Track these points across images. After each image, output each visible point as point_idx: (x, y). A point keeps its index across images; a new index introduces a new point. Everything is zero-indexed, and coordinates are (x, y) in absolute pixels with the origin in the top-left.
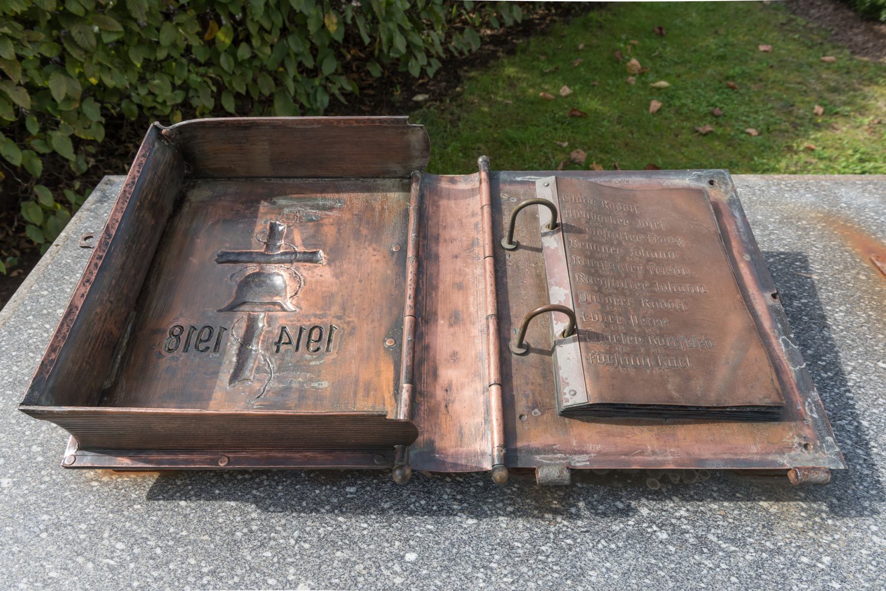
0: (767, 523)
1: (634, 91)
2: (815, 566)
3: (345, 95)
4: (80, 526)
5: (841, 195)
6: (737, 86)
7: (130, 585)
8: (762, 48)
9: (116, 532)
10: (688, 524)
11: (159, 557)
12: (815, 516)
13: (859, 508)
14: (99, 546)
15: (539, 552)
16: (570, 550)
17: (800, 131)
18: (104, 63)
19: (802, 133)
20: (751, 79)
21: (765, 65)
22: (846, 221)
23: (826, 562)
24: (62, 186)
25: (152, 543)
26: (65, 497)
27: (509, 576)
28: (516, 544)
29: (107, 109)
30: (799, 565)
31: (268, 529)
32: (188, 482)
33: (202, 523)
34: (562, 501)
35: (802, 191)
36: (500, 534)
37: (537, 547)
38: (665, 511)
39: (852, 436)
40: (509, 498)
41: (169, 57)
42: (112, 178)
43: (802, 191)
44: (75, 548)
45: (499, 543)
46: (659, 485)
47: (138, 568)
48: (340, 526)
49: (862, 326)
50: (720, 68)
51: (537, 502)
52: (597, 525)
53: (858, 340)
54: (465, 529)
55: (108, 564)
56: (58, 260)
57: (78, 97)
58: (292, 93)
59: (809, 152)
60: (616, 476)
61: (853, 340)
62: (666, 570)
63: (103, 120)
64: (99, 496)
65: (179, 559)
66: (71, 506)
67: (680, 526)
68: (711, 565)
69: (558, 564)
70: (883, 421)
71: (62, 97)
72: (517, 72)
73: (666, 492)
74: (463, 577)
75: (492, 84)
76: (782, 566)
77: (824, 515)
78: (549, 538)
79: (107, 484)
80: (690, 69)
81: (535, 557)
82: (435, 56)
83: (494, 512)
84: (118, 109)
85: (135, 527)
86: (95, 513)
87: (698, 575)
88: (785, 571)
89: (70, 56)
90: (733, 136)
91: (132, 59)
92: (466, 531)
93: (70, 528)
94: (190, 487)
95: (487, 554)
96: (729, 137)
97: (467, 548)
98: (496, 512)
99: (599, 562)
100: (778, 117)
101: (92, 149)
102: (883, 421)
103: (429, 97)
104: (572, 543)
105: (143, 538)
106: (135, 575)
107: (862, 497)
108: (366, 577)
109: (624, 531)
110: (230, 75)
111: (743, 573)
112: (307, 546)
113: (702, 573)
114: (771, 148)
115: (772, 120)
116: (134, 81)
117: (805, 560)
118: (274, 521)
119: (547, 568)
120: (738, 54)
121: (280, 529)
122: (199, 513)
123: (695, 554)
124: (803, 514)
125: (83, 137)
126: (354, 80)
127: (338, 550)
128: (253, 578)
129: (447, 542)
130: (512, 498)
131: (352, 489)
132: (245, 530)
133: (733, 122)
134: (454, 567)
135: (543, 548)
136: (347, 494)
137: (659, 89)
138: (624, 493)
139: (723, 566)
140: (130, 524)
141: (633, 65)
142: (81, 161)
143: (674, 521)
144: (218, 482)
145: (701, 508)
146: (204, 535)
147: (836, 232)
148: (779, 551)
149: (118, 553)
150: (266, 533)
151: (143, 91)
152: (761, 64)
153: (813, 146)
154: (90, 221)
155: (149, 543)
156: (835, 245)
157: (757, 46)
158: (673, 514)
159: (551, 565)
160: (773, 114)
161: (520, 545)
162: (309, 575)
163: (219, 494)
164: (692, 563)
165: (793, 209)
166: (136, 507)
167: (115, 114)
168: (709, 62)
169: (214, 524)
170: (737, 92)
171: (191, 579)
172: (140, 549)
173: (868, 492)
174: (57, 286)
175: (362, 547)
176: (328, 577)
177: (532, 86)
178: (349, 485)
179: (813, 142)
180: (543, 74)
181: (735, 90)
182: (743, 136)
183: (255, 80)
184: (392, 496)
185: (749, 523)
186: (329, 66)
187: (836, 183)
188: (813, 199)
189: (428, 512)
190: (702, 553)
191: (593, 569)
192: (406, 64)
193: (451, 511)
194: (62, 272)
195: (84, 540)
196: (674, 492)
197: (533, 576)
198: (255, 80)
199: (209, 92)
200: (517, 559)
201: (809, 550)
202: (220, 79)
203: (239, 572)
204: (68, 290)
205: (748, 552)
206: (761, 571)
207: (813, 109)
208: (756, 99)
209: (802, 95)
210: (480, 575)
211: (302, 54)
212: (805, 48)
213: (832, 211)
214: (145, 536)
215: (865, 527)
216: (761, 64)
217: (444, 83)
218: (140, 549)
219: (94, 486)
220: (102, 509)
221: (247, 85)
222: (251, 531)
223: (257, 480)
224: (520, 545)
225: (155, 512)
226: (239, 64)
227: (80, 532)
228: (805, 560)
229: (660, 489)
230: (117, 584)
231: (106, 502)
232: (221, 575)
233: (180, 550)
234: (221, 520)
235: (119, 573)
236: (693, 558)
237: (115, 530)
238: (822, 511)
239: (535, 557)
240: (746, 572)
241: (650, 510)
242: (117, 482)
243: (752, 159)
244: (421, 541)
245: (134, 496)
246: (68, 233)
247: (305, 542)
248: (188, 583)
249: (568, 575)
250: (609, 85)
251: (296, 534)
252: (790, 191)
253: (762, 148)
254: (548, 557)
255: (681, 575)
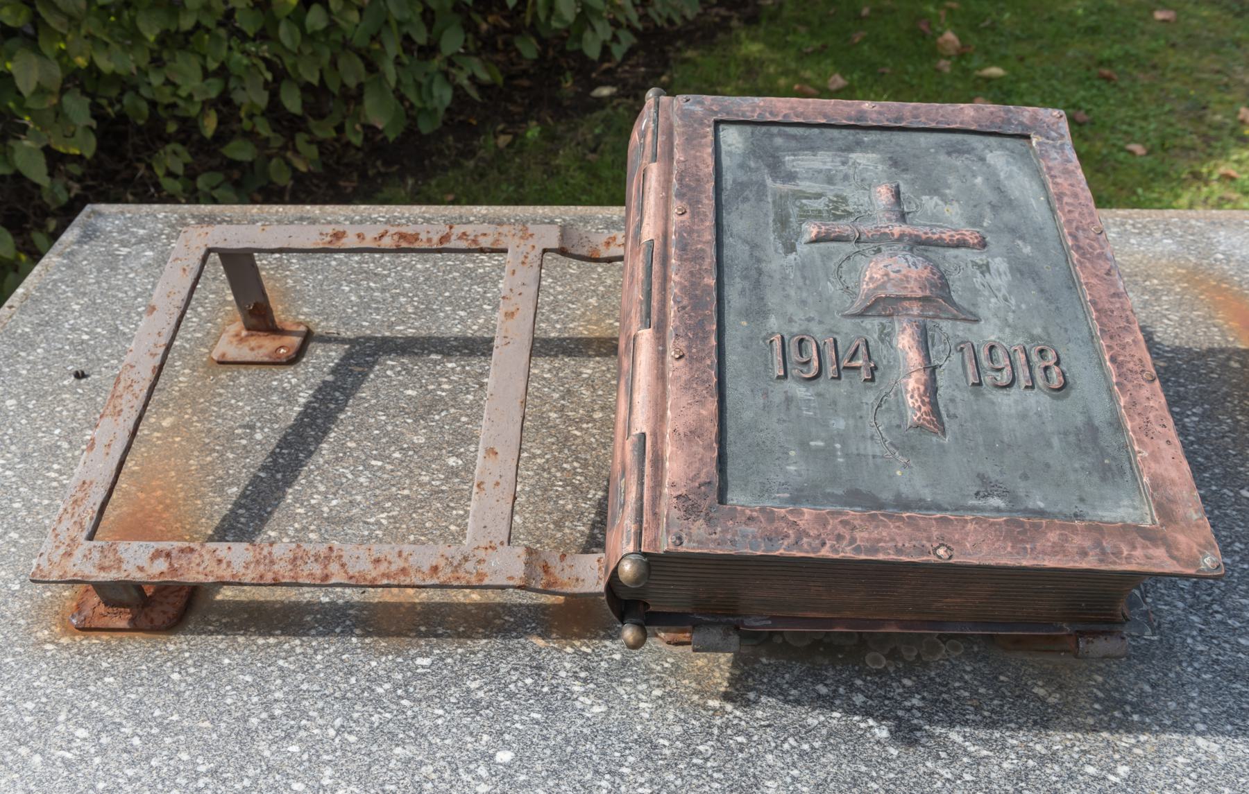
0: (1041, 719)
1: (948, 82)
2: (1104, 778)
3: (481, 87)
4: (25, 705)
5: (1218, 242)
6: (1115, 77)
7: (93, 787)
8: (1159, 15)
9: (76, 714)
10: (921, 718)
11: (137, 750)
12: (1115, 709)
13: (1182, 699)
14: (52, 733)
15: (694, 753)
16: (741, 751)
17: (1216, 148)
18: (98, 35)
19: (1218, 151)
20: (1139, 65)
21: (1162, 42)
22: (1221, 280)
23: (1122, 774)
24: (28, 226)
25: (128, 730)
26: (5, 665)
27: (647, 785)
28: (661, 741)
29: (100, 107)
30: (1080, 778)
31: (298, 714)
32: (185, 646)
33: (202, 705)
34: (736, 683)
35: (1158, 235)
36: (639, 728)
37: (692, 747)
38: (889, 699)
39: (1187, 596)
40: (658, 677)
41: (198, 26)
42: (102, 207)
43: (1158, 235)
44: (17, 735)
45: (636, 740)
46: (884, 662)
47: (106, 764)
48: (404, 712)
49: (1223, 437)
50: (1089, 48)
51: (699, 684)
52: (786, 716)
53: (1214, 457)
54: (588, 719)
55: (63, 758)
56: (11, 328)
57: (56, 88)
58: (393, 83)
59: (1228, 182)
60: (821, 649)
61: (1207, 458)
62: (880, 782)
63: (94, 124)
64: (55, 664)
65: (165, 753)
66: (13, 677)
67: (909, 720)
68: (949, 776)
69: (720, 771)
70: (1236, 575)
71: (32, 87)
72: (760, 51)
73: (895, 672)
74: (578, 785)
75: (718, 70)
76: (1054, 779)
77: (1128, 708)
78: (712, 734)
79: (67, 648)
80: (1041, 48)
81: (688, 760)
82: (625, 26)
83: (632, 696)
84: (118, 107)
85: (104, 708)
86: (48, 688)
87: (928, 789)
88: (1059, 786)
89: (46, 25)
90: (1105, 156)
91: (142, 30)
92: (589, 722)
93: (10, 707)
94: (187, 655)
95: (617, 754)
96: (1099, 157)
97: (588, 746)
98: (637, 697)
99: (783, 769)
100: (1179, 126)
101: (76, 169)
102: (1236, 575)
103: (618, 92)
104: (745, 741)
105: (114, 723)
106: (100, 773)
107: (1188, 683)
108: (436, 784)
109: (824, 726)
110: (295, 55)
111: (995, 787)
112: (352, 739)
113: (935, 786)
114: (1165, 175)
115: (1169, 130)
116: (144, 62)
117: (1091, 770)
118: (307, 704)
119: (704, 776)
120: (1119, 25)
121: (314, 714)
122: (199, 690)
123: (927, 759)
124: (1097, 706)
125: (61, 149)
126: (497, 63)
127: (397, 745)
128: (271, 781)
129: (559, 738)
130: (662, 678)
131: (426, 661)
132: (264, 715)
133: (1107, 133)
134: (567, 772)
135: (701, 748)
136: (417, 668)
137: (988, 80)
138: (831, 673)
139: (967, 777)
140: (97, 704)
141: (947, 41)
142: (59, 187)
143: (900, 713)
144: (228, 648)
145: (945, 696)
146: (203, 721)
147: (1202, 297)
148: (1054, 758)
149: (78, 743)
150: (293, 719)
151: (156, 79)
152: (1157, 40)
153: (1233, 173)
154: (61, 271)
155: (123, 730)
156: (1199, 316)
157: (1152, 11)
158: (900, 704)
159: (710, 772)
160: (1173, 120)
161: (667, 743)
162: (353, 779)
163: (230, 664)
164: (921, 772)
165: (1141, 262)
166: (107, 680)
167: (113, 115)
168: (1072, 38)
169: (220, 705)
170: (1115, 86)
171: (181, 781)
172: (109, 738)
173: (1198, 676)
174: (8, 366)
175: (433, 742)
176: (380, 782)
177: (785, 73)
178: (421, 656)
179: (1235, 166)
180: (802, 56)
181: (1112, 83)
182: (1122, 156)
183: (334, 63)
184: (484, 671)
185: (1013, 717)
186: (452, 42)
187: (1213, 223)
188: (1174, 247)
189: (535, 695)
190: (938, 758)
191: (772, 778)
192: (579, 38)
193: (568, 695)
194: (16, 345)
195: (31, 724)
196: (905, 673)
197: (682, 787)
198: (334, 63)
199: (261, 79)
200: (661, 762)
201: (1099, 756)
202: (278, 62)
203: (251, 772)
204: (24, 372)
205: (1006, 759)
206: (1023, 784)
207: (1238, 113)
208: (1146, 97)
209: (1221, 91)
210: (604, 783)
211: (409, 22)
212: (1230, 16)
213: (1201, 265)
214: (118, 720)
215: (1188, 725)
216: (1157, 40)
217: (643, 69)
218: (109, 738)
219: (48, 651)
220: (58, 682)
221: (321, 71)
222: (272, 717)
223: (286, 646)
224: (667, 743)
225: (135, 688)
226: (308, 37)
227: (25, 712)
228: (1091, 770)
229: (885, 667)
230: (75, 785)
231: (64, 673)
232: (225, 775)
233: (168, 740)
234: (229, 701)
235: (79, 771)
236: (924, 765)
237: (75, 711)
238: (1126, 703)
239: (688, 760)
240: (1000, 786)
241: (866, 697)
242: (82, 645)
243: (1135, 193)
244: (520, 736)
245: (105, 665)
246: (27, 289)
247: (350, 733)
248: (176, 786)
249: (735, 786)
250: (907, 73)
251: (338, 722)
252: (1139, 234)
253: (1151, 175)
254: (707, 760)
255: (903, 788)
